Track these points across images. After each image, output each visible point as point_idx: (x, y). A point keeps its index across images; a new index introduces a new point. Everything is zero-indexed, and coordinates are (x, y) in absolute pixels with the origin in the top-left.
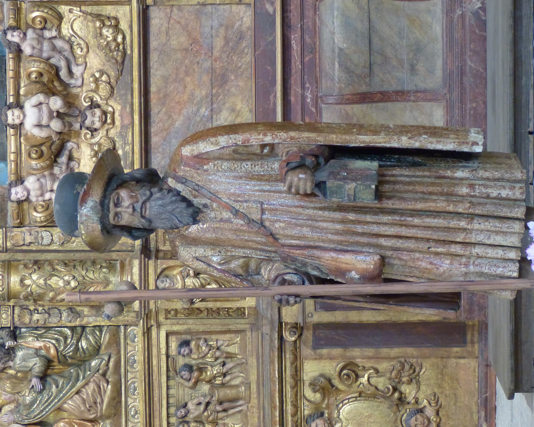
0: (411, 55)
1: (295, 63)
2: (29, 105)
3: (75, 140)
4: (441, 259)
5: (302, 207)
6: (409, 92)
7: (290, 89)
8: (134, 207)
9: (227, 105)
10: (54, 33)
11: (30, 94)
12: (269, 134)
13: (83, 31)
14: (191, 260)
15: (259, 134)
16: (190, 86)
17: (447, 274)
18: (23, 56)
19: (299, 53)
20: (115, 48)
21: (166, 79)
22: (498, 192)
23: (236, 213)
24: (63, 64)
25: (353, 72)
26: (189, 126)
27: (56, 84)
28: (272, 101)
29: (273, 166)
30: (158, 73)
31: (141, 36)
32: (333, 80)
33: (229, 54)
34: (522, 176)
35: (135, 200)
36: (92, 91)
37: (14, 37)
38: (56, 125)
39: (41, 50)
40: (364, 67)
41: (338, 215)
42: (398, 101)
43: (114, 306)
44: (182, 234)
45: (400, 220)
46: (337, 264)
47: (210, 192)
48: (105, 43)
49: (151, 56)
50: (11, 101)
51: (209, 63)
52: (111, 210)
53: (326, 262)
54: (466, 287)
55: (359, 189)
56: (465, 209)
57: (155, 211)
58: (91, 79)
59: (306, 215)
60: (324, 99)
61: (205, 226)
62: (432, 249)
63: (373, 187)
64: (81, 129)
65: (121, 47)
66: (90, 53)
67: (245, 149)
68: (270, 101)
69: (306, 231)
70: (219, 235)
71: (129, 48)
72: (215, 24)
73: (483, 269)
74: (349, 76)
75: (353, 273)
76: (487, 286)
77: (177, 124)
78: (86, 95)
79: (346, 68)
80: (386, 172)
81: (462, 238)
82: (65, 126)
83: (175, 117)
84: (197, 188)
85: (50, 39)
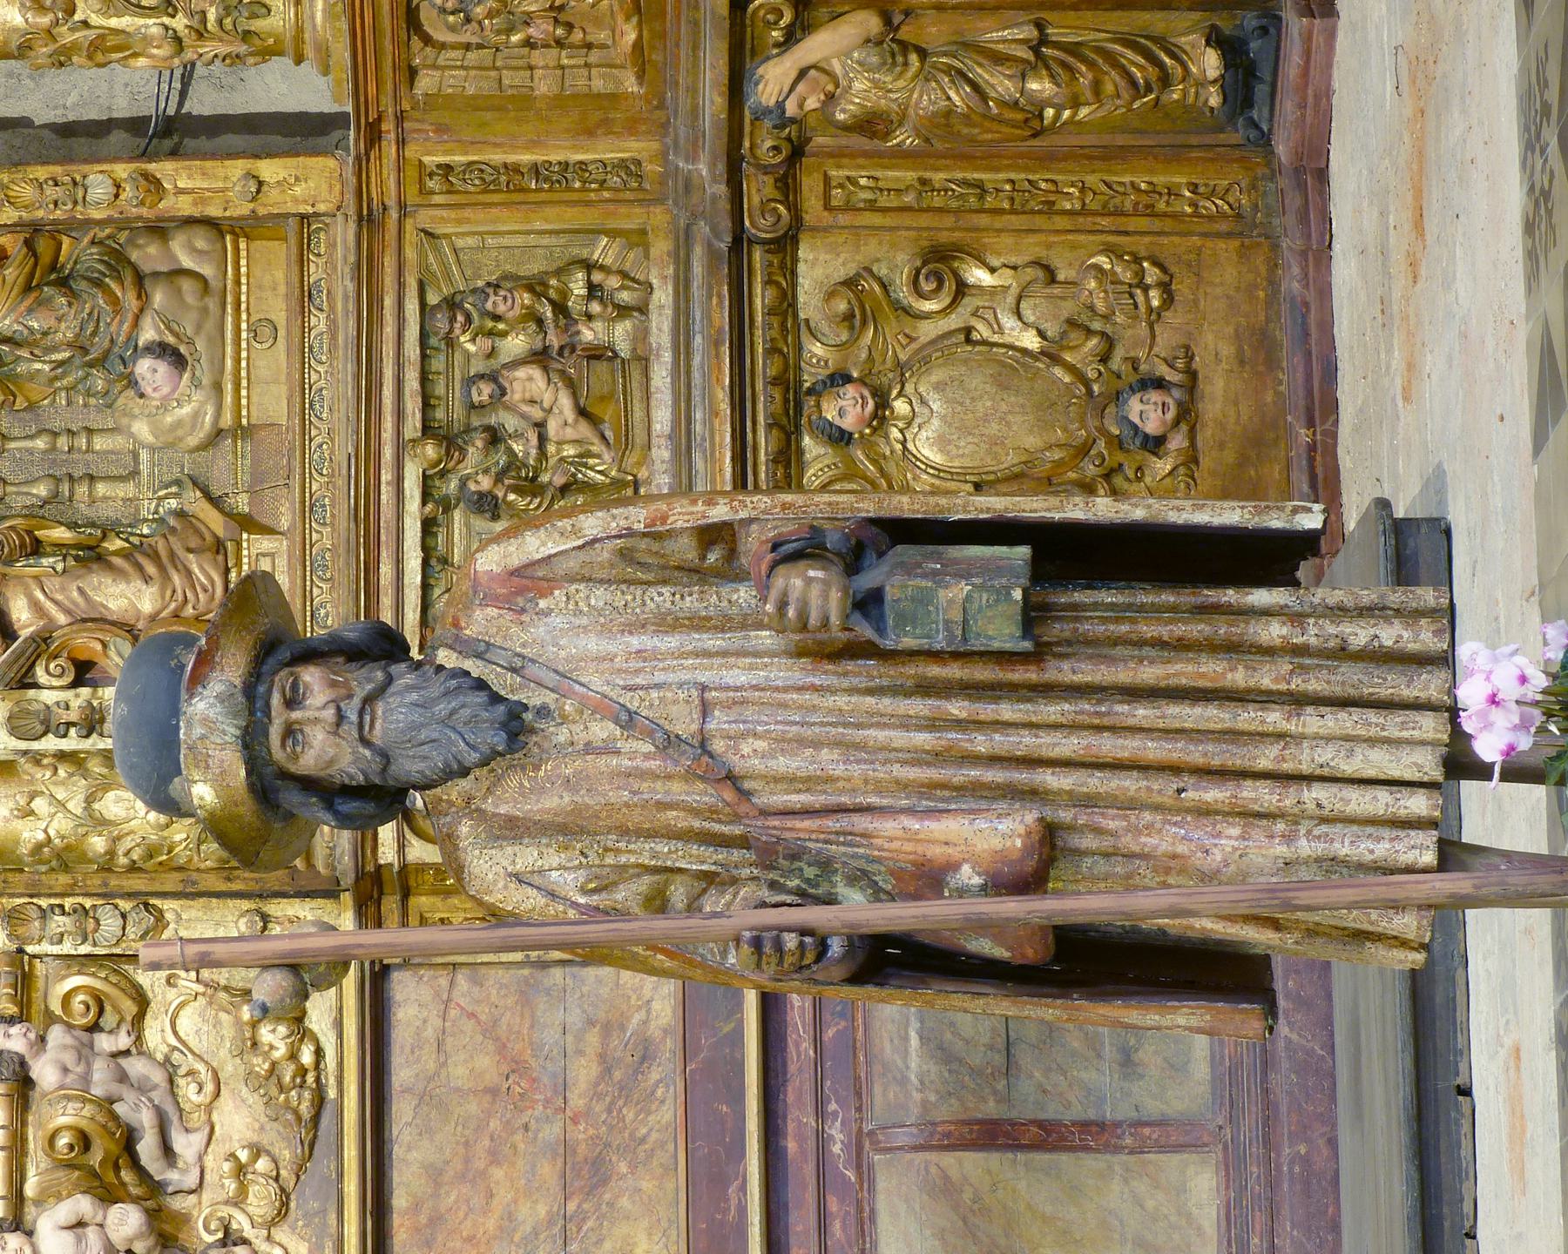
1: (797, 1045)
4: (1214, 825)
5: (815, 688)
6: (1117, 1125)
7: (785, 1117)
8: (339, 709)
10: (124, 1041)
11: (50, 1195)
12: (722, 501)
13: (204, 1037)
14: (500, 885)
15: (694, 502)
16: (502, 1192)
17: (1233, 867)
18: (35, 1095)
19: (809, 1016)
20: (293, 1078)
21: (435, 1175)
22: (1372, 631)
23: (629, 721)
25: (960, 1061)
27: (127, 1176)
31: (368, 1046)
32: (903, 1081)
33: (612, 1103)
34: (1436, 598)
35: (343, 691)
36: (226, 1203)
37: (15, 1040)
39: (86, 1079)
41: (919, 707)
42: (1086, 1149)
43: (279, 977)
44: (478, 810)
46: (920, 849)
47: (556, 671)
48: (266, 1066)
49: (394, 1109)
53: (886, 846)
54: (1291, 894)
57: (398, 722)
58: (227, 1166)
59: (830, 711)
60: (881, 1137)
61: (542, 773)
63: (1017, 594)
65: (310, 1078)
66: (222, 1099)
67: (655, 547)
69: (829, 760)
71: (332, 1081)
72: (575, 1018)
74: (950, 1071)
75: (966, 869)
76: (1349, 891)
78: (211, 1214)
79: (941, 1048)
80: (1053, 599)
81: (1272, 756)
84: (518, 663)
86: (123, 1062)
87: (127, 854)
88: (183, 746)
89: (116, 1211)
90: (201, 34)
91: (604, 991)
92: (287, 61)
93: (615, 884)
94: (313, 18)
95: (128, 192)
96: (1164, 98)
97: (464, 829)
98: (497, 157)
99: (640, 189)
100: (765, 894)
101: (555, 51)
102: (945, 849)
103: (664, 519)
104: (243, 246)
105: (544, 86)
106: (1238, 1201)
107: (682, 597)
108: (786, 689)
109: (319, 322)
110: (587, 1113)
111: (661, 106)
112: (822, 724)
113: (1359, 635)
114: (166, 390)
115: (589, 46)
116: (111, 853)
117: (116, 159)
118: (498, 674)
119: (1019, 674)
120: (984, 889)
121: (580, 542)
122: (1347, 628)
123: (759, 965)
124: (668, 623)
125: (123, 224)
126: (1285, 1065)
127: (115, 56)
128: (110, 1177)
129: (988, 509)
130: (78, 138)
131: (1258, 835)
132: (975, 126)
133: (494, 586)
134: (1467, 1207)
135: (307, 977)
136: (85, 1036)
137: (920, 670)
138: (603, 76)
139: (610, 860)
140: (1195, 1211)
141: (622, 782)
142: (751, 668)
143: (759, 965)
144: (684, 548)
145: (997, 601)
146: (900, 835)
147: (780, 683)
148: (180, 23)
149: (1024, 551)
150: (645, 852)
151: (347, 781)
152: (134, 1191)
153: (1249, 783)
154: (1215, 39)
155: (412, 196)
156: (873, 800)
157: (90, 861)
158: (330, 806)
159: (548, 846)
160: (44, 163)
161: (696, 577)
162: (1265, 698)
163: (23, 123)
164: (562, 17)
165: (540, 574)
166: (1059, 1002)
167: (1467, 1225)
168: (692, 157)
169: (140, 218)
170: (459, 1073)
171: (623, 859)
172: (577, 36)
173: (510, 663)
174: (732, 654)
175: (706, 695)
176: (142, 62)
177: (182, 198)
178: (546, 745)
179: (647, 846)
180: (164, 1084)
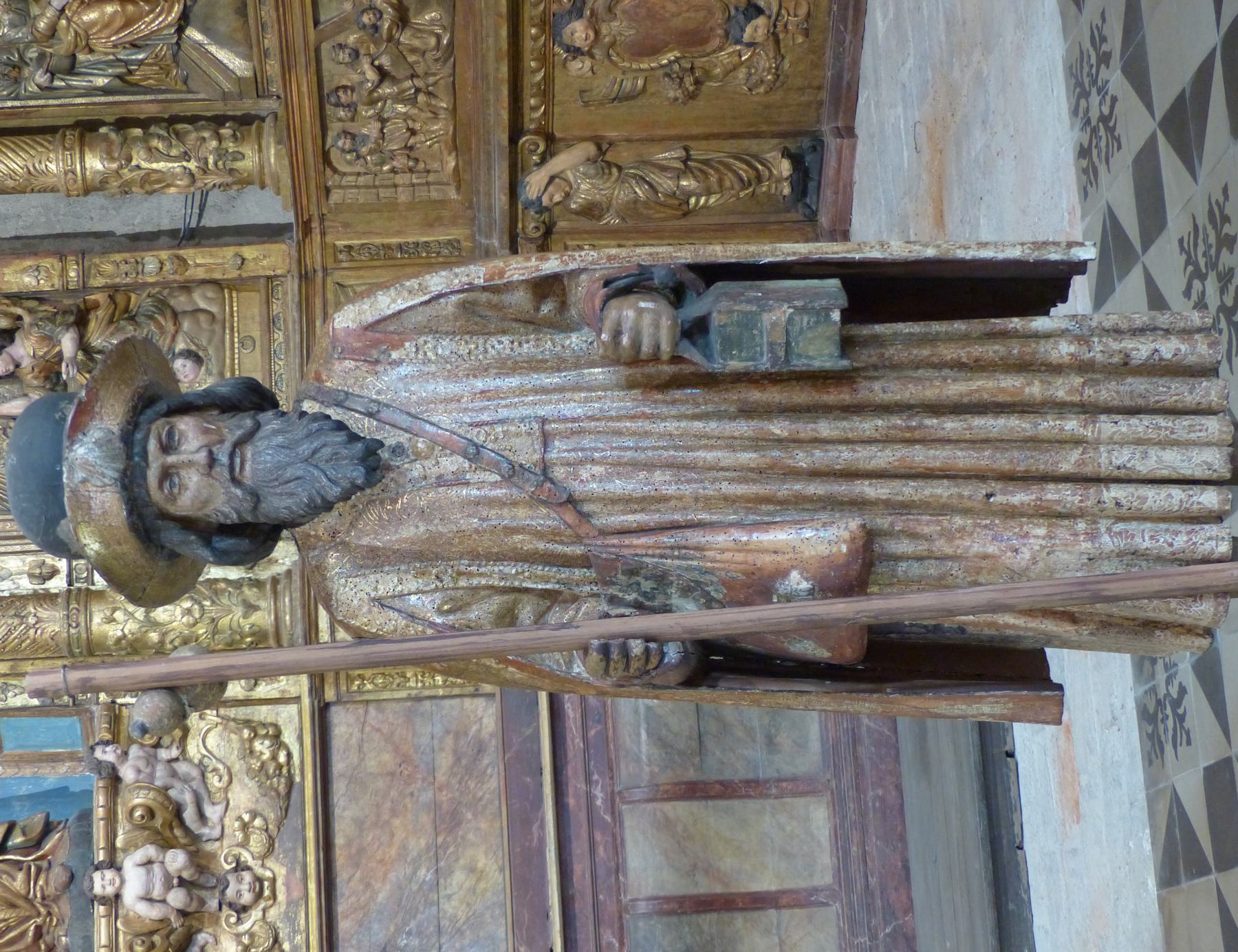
0: (766, 721)
2: (130, 864)
3: (210, 930)
4: (1021, 526)
5: (645, 416)
6: (767, 781)
8: (211, 453)
9: (462, 862)
10: (175, 752)
14: (365, 609)
17: (1041, 564)
18: (122, 786)
19: (579, 723)
21: (359, 824)
22: (1153, 346)
23: (474, 453)
24: (188, 798)
25: (672, 747)
26: (401, 899)
27: (178, 832)
28: (536, 835)
29: (568, 342)
30: (347, 813)
32: (638, 760)
33: (462, 778)
34: (1202, 318)
35: (215, 437)
36: (238, 845)
38: (177, 898)
39: (152, 776)
40: (690, 738)
41: (743, 428)
42: (748, 796)
44: (343, 543)
45: (909, 428)
46: (750, 558)
47: (409, 414)
50: (101, 858)
51: (430, 794)
52: (150, 458)
53: (719, 557)
55: (797, 328)
56: (1070, 392)
57: (266, 462)
59: (661, 436)
61: (398, 506)
62: (998, 499)
64: (220, 909)
65: (285, 771)
67: (495, 299)
68: (531, 834)
69: (662, 481)
70: (439, 527)
71: (297, 771)
72: (438, 730)
73: (1138, 540)
75: (795, 575)
76: (1155, 581)
77: (381, 897)
79: (660, 739)
81: (1073, 461)
82: (192, 899)
83: (377, 886)
85: (170, 761)
86: (175, 765)
87: (172, 642)
88: (67, 490)
89: (171, 853)
90: (205, 171)
91: (455, 713)
92: (256, 187)
93: (469, 604)
94: (269, 159)
95: (168, 266)
96: (758, 191)
97: (332, 559)
98: (378, 241)
99: (460, 255)
100: (604, 607)
101: (409, 175)
102: (774, 557)
103: (501, 274)
104: (234, 295)
105: (403, 197)
106: (842, 826)
107: (520, 344)
108: (619, 418)
109: (279, 336)
110: (447, 785)
111: (471, 207)
112: (655, 448)
113: (1141, 350)
114: (191, 377)
115: (428, 172)
116: (162, 642)
117: (162, 249)
118: (356, 419)
119: (832, 396)
120: (811, 593)
121: (426, 298)
122: (1128, 344)
123: (606, 671)
124: (507, 366)
125: (165, 284)
126: (867, 741)
127: (157, 186)
128: (167, 833)
129: (794, 254)
130: (141, 240)
131: (1062, 533)
132: (650, 209)
133: (351, 340)
134: (1017, 829)
135: (185, 699)
136: (152, 751)
137: (742, 396)
138: (437, 190)
139: (463, 583)
140: (815, 832)
141: (472, 510)
142: (586, 400)
143: (606, 671)
144: (520, 299)
145: (817, 323)
146: (727, 546)
147: (613, 413)
148: (192, 165)
149: (834, 284)
150: (494, 574)
151: (222, 520)
152: (183, 841)
153: (1051, 486)
154: (786, 154)
155: (330, 264)
156: (704, 516)
157: (151, 648)
158: (208, 543)
159: (406, 572)
160: (119, 252)
161: (531, 328)
162: (1062, 408)
163: (109, 234)
164: (413, 155)
165: (392, 328)
166: (875, 696)
167: (1018, 841)
168: (489, 236)
169: (175, 281)
170: (371, 764)
171: (475, 582)
172: (421, 166)
173: (366, 408)
174: (569, 390)
175: (547, 427)
176: (172, 190)
177: (199, 269)
178: (401, 480)
179: (496, 569)
180: (199, 777)
